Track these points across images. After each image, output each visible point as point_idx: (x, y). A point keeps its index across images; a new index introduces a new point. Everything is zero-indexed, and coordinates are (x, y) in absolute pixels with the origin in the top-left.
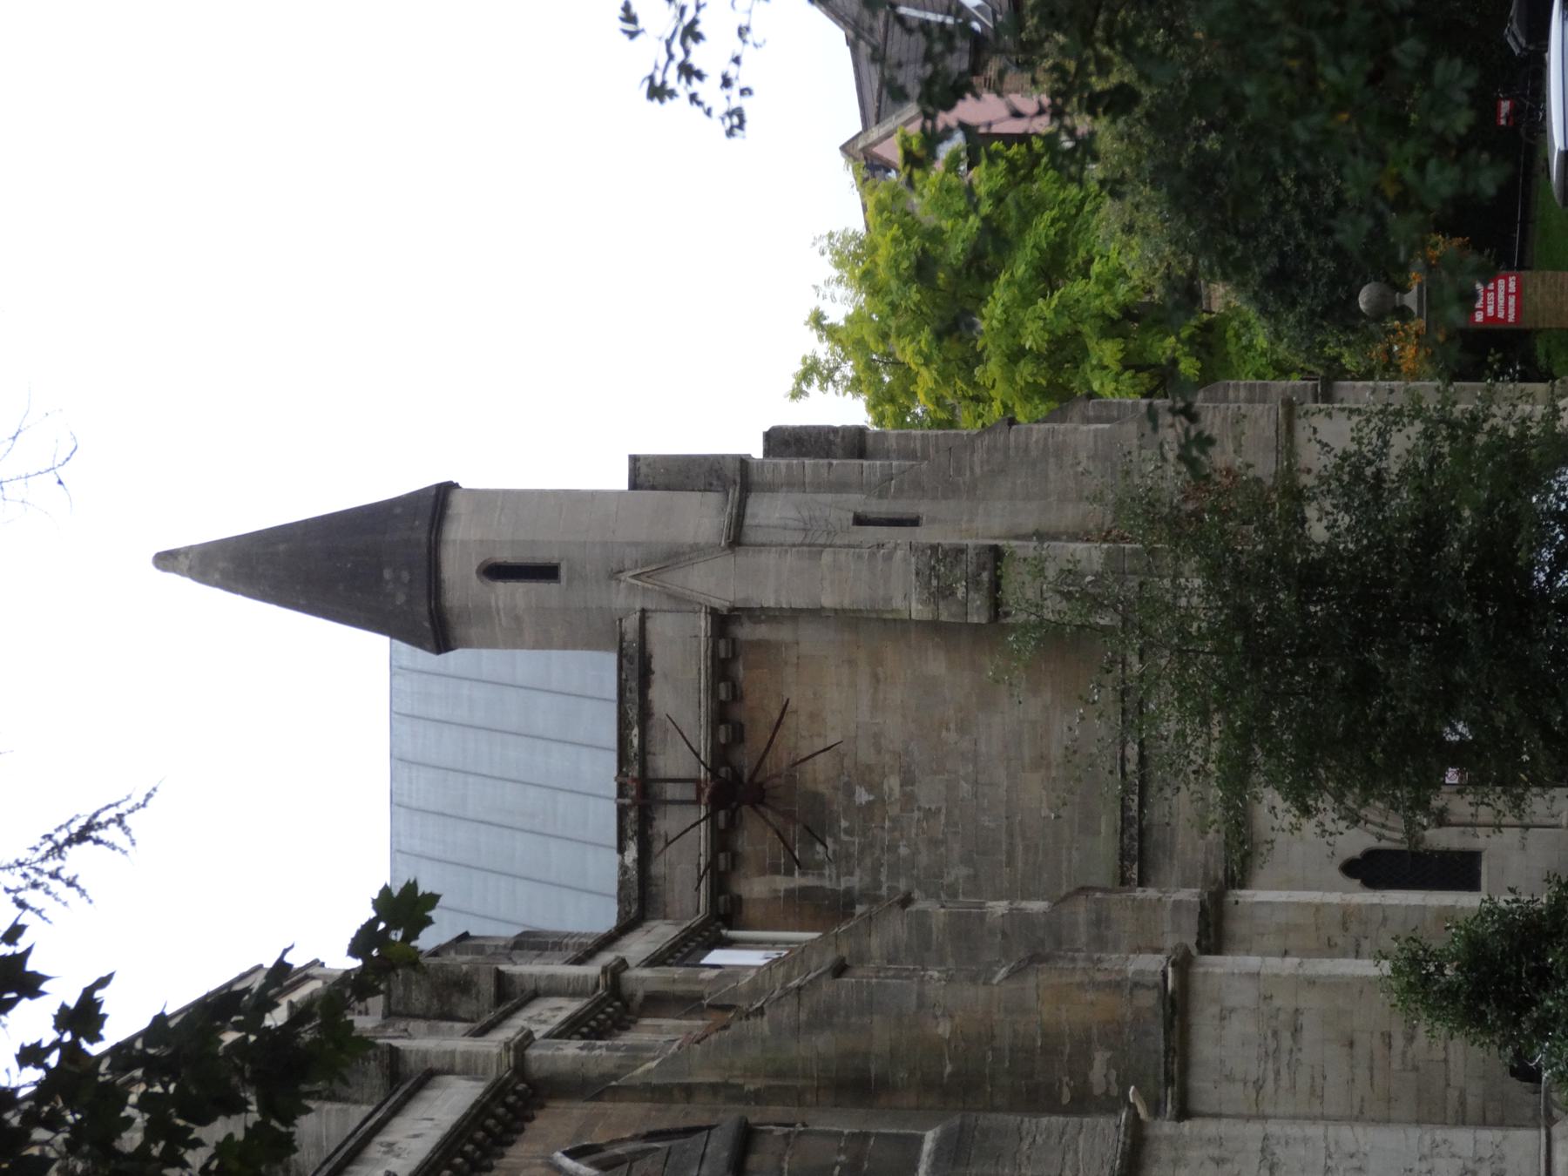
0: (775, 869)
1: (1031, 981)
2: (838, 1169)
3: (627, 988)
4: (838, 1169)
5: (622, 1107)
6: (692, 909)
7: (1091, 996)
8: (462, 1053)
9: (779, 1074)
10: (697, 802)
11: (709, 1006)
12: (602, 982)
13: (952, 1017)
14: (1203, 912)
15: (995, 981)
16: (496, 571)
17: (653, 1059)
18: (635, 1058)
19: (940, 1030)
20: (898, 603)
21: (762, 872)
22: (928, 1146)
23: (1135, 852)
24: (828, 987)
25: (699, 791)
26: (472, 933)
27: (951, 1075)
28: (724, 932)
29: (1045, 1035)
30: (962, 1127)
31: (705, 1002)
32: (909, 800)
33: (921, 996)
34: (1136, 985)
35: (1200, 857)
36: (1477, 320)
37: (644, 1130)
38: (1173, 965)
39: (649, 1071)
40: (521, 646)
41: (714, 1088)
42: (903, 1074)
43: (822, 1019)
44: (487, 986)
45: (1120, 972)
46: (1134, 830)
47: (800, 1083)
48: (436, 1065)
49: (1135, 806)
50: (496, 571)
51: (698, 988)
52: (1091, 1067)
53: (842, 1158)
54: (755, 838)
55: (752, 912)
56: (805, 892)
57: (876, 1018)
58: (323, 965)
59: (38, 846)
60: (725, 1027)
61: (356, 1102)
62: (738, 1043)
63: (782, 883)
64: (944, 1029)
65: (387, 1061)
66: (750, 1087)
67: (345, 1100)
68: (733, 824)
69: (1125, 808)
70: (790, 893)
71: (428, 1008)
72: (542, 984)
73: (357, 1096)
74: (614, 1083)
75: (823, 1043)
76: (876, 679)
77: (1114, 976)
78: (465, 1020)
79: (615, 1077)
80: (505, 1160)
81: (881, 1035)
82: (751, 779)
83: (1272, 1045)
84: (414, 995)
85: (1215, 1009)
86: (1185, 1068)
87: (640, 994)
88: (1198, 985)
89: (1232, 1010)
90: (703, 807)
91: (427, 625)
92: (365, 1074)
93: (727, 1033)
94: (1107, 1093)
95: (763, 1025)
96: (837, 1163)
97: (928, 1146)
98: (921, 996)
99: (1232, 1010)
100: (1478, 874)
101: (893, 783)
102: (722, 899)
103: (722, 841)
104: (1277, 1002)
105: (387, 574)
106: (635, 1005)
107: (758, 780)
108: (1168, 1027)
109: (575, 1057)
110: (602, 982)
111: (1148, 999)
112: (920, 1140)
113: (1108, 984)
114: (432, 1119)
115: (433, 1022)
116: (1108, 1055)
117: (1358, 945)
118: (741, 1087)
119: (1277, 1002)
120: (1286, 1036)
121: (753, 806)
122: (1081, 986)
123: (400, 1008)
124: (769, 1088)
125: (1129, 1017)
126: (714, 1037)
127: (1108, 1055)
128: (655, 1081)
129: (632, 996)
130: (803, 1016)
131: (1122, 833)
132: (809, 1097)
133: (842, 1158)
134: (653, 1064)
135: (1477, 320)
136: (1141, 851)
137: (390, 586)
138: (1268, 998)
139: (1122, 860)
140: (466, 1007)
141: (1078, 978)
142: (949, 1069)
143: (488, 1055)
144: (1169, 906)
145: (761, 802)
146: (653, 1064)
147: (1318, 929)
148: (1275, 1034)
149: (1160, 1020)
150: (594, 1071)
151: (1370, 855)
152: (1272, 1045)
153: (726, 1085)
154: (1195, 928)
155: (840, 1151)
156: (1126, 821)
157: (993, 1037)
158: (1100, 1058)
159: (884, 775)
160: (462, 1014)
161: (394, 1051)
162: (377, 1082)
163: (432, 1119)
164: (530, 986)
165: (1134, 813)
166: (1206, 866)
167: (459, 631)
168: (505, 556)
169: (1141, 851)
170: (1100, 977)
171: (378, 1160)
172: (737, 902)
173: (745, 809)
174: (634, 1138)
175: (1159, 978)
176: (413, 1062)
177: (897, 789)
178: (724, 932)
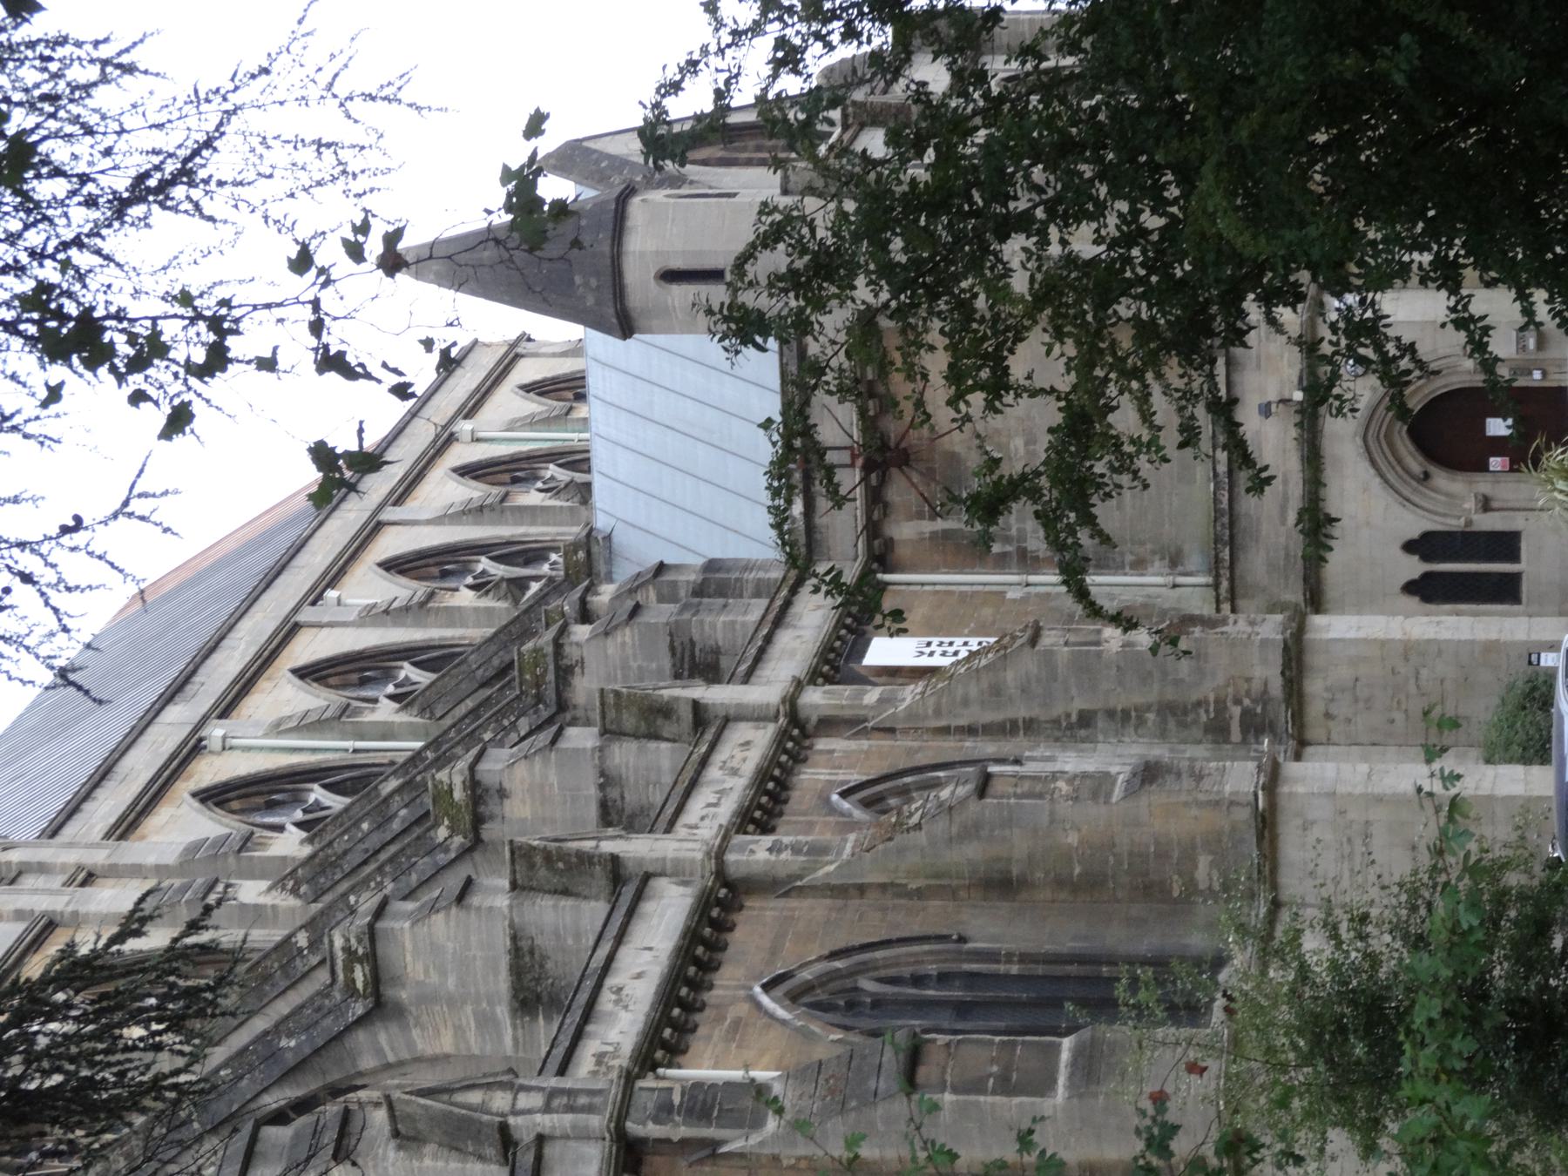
0: (920, 516)
1: (1144, 800)
2: (991, 1081)
3: (803, 714)
4: (991, 1081)
5: (807, 903)
6: (851, 553)
7: (1194, 812)
8: (672, 860)
9: (937, 876)
10: (852, 465)
11: (873, 729)
12: (782, 709)
13: (1079, 830)
14: (1286, 649)
15: (1114, 800)
16: (671, 276)
17: (831, 863)
18: (816, 862)
19: (1069, 840)
21: (910, 518)
22: (1065, 1056)
23: (1226, 538)
24: (974, 806)
25: (854, 457)
26: (666, 562)
27: (1080, 875)
28: (879, 576)
29: (1157, 843)
30: (1093, 1038)
31: (870, 724)
33: (1052, 813)
34: (1232, 803)
35: (1282, 540)
36: (1492, 459)
37: (826, 952)
38: (1263, 789)
39: (828, 874)
40: (695, 332)
41: (883, 887)
42: (1039, 875)
43: (971, 832)
44: (686, 714)
45: (1218, 792)
46: (1226, 520)
47: (955, 882)
48: (651, 870)
49: (1225, 500)
50: (671, 276)
51: (862, 712)
52: (1196, 867)
53: (995, 1069)
54: (900, 491)
55: (902, 552)
56: (947, 534)
57: (1016, 831)
58: (529, 340)
59: (265, 64)
60: (890, 839)
61: (585, 898)
62: (901, 851)
63: (928, 527)
64: (1073, 839)
65: (609, 867)
66: (913, 886)
67: (577, 895)
68: (883, 481)
69: (1216, 501)
70: (934, 536)
71: (637, 728)
72: (732, 712)
73: (586, 893)
74: (799, 883)
75: (972, 852)
77: (1213, 797)
78: (667, 740)
79: (801, 877)
80: (714, 992)
81: (1018, 847)
82: (898, 445)
83: (1347, 849)
84: (625, 716)
85: (1299, 822)
86: (1274, 870)
87: (814, 719)
88: (1283, 802)
89: (1313, 823)
90: (857, 471)
91: (614, 320)
92: (592, 876)
93: (891, 844)
94: (1210, 888)
95: (921, 838)
96: (990, 1075)
97: (1065, 1056)
98: (1052, 813)
99: (1313, 823)
100: (1519, 549)
102: (876, 543)
103: (876, 498)
104: (1352, 815)
105: (578, 280)
106: (810, 727)
107: (903, 445)
108: (1260, 837)
109: (767, 862)
110: (782, 709)
111: (1243, 814)
112: (1056, 1048)
113: (1209, 803)
114: (650, 949)
115: (644, 741)
116: (1210, 858)
117: (1418, 673)
118: (905, 885)
119: (1352, 815)
120: (1358, 842)
121: (900, 467)
122: (1186, 804)
123: (614, 727)
124: (929, 887)
125: (1227, 828)
126: (881, 847)
127: (1210, 858)
128: (833, 882)
129: (808, 720)
130: (954, 830)
131: (1215, 521)
132: (963, 894)
133: (995, 1069)
134: (831, 868)
135: (1506, 432)
136: (1232, 537)
137: (581, 290)
138: (1343, 813)
139: (1216, 542)
140: (668, 729)
141: (1183, 798)
142: (1077, 871)
143: (693, 861)
144: (1257, 643)
145: (907, 465)
146: (831, 868)
147: (1383, 659)
148: (1349, 840)
149: (1253, 831)
150: (782, 873)
151: (1427, 536)
152: (1347, 849)
153: (892, 884)
154: (1280, 661)
155: (993, 1061)
156: (1218, 513)
157: (1114, 845)
158: (1204, 862)
159: (1009, 436)
160: (665, 735)
161: (615, 859)
162: (603, 882)
163: (650, 949)
164: (722, 713)
165: (1225, 505)
166: (1286, 548)
167: (640, 322)
168: (678, 264)
169: (1232, 537)
170: (1202, 797)
171: (611, 1014)
172: (889, 544)
173: (894, 471)
174: (818, 960)
175: (1251, 798)
176: (631, 867)
177: (1022, 451)
178: (879, 576)
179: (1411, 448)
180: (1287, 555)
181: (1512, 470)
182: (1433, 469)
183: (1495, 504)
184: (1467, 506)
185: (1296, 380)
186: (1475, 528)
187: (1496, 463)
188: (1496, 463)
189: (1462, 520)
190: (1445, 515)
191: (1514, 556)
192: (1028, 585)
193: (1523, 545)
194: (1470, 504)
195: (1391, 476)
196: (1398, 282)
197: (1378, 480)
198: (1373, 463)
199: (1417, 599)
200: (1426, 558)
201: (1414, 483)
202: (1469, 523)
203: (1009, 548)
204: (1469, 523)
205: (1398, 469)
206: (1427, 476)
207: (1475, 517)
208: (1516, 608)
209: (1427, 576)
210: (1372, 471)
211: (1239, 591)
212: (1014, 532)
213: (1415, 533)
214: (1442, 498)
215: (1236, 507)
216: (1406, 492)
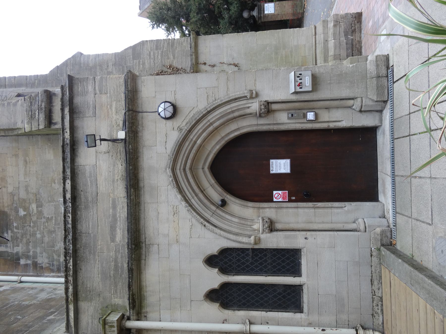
20: (19, 125)
32: (40, 213)
35: (112, 254)
76: (26, 161)
100: (299, 264)
101: (34, 206)
135: (294, 199)
151: (224, 252)
159: (30, 203)
179: (213, 181)
180: (116, 266)
181: (290, 201)
182: (229, 198)
183: (278, 226)
184: (255, 227)
185: (121, 123)
186: (262, 246)
187: (278, 195)
188: (278, 195)
189: (252, 238)
190: (237, 234)
191: (297, 272)
192: (21, 282)
193: (304, 261)
194: (258, 225)
195: (194, 202)
196: (208, 293)
197: (184, 203)
198: (180, 191)
199: (217, 305)
200: (224, 271)
201: (214, 208)
202: (258, 241)
203: (29, 262)
204: (258, 241)
205: (201, 196)
206: (224, 203)
207: (263, 236)
208: (298, 316)
209: (225, 286)
210: (179, 196)
211: (82, 295)
212: (31, 253)
213: (214, 249)
214: (236, 220)
215: (79, 227)
216: (207, 215)
